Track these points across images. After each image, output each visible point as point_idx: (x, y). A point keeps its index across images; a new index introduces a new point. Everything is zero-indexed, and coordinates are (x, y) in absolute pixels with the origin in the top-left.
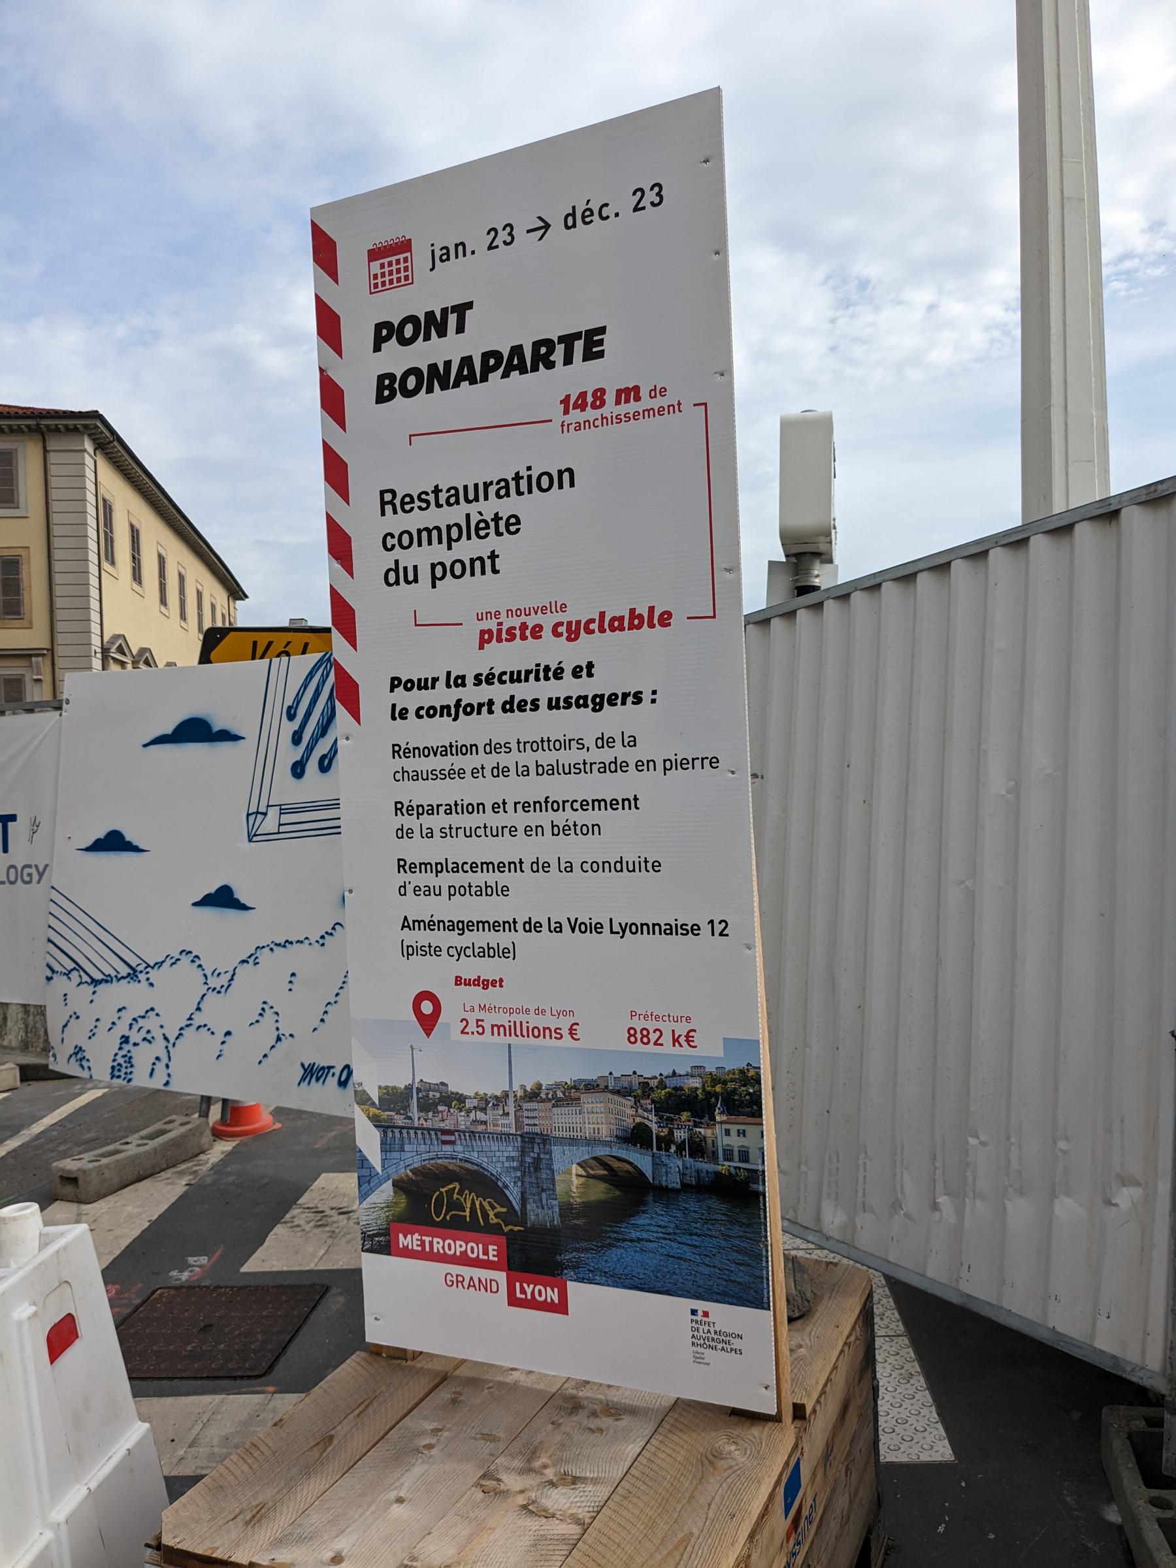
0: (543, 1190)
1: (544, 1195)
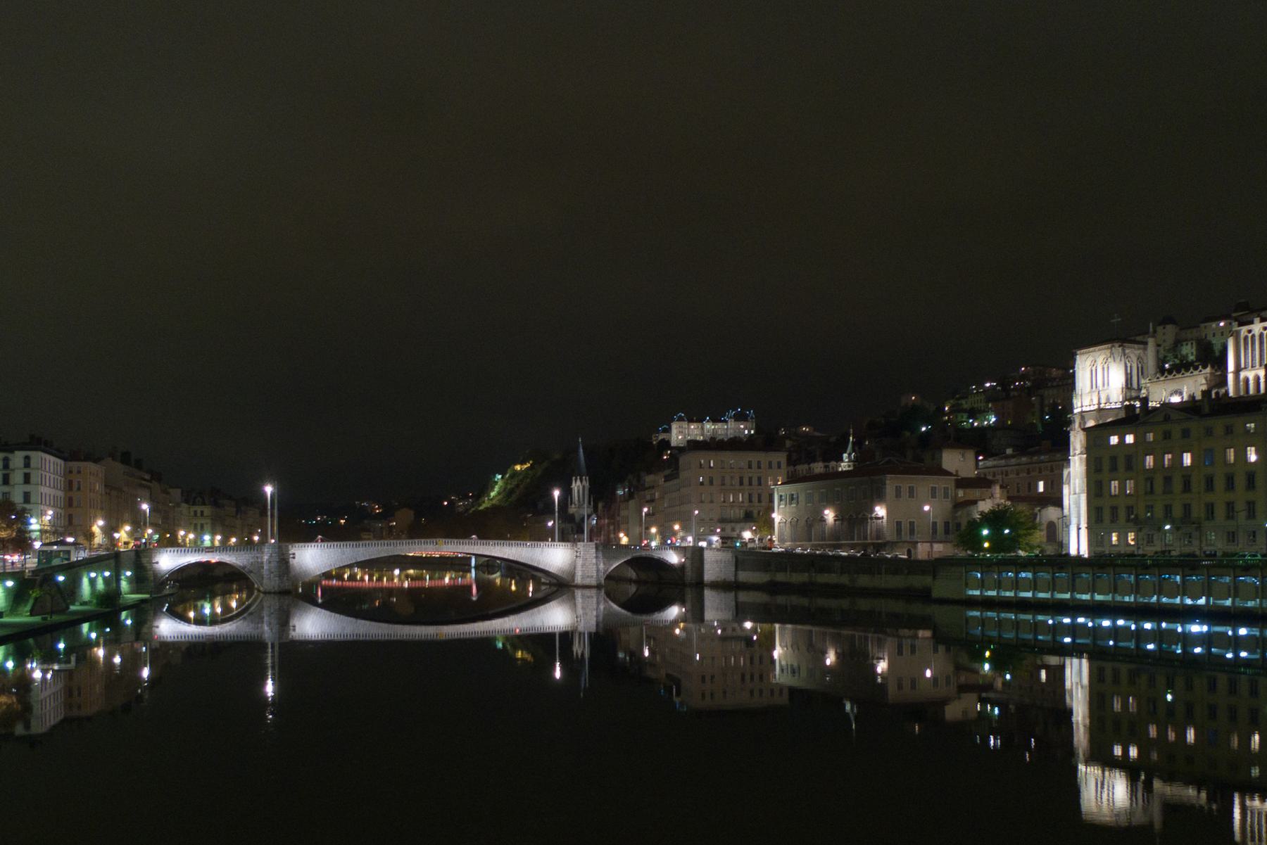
0: (272, 573)
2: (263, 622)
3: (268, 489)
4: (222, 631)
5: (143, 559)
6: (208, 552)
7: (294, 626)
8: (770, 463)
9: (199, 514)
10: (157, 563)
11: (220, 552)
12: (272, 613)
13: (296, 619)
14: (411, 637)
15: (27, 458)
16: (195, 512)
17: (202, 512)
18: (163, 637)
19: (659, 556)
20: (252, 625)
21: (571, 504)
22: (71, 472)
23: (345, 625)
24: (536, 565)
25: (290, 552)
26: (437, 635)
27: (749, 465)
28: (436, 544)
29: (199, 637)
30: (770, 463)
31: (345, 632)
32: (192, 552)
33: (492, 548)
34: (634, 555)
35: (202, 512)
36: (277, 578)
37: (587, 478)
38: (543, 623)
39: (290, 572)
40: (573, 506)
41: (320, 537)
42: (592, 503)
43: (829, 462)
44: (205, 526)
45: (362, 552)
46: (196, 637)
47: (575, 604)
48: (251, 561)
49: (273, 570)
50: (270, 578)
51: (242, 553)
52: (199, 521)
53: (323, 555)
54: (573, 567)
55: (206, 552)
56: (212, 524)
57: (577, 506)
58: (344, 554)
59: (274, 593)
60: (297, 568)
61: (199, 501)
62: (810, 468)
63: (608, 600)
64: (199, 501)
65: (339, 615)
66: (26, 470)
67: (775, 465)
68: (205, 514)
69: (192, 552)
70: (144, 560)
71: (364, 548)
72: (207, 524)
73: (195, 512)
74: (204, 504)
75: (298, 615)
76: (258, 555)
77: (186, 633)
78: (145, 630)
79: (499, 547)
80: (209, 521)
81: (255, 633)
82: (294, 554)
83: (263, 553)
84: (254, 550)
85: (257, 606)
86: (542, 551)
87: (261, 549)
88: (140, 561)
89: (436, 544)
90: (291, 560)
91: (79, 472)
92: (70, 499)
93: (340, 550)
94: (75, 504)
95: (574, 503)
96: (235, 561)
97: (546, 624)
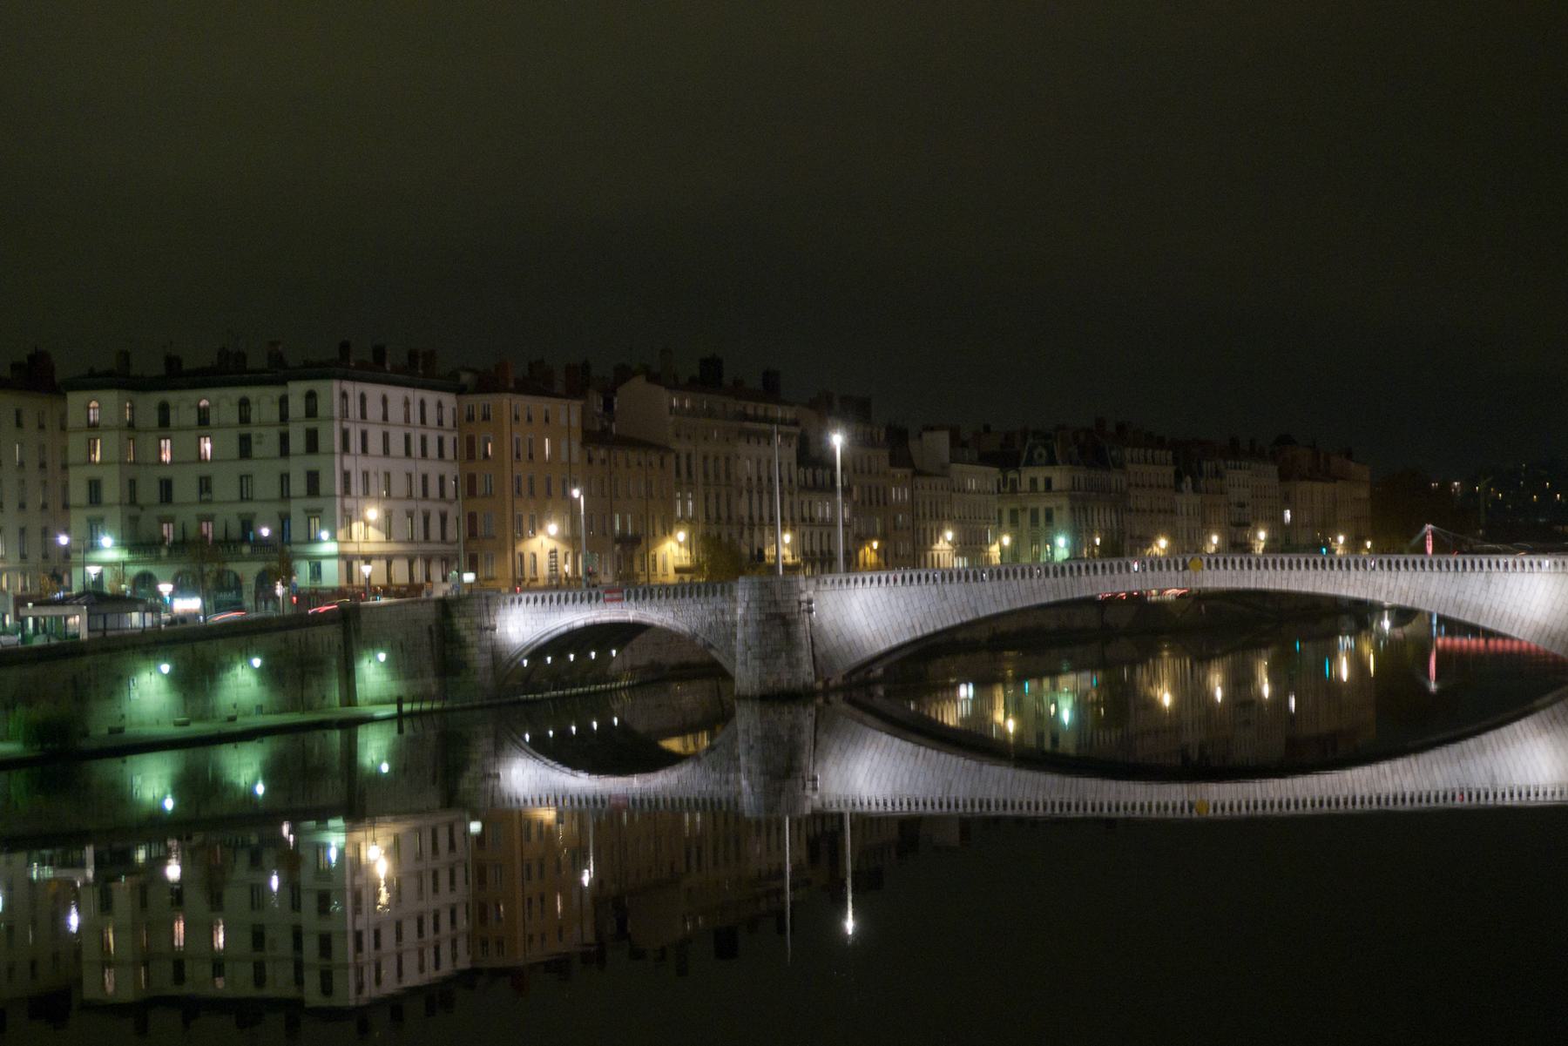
0: (750, 649)
1: (749, 652)
2: (738, 770)
3: (838, 441)
4: (647, 786)
5: (456, 620)
6: (612, 600)
7: (815, 779)
9: (1041, 485)
11: (636, 598)
12: (752, 747)
13: (830, 761)
14: (1549, 797)
15: (244, 403)
16: (1034, 481)
17: (1048, 482)
18: (518, 801)
20: (715, 776)
22: (470, 418)
23: (950, 777)
24: (1468, 619)
26: (1191, 806)
27: (439, 421)
28: (1185, 567)
29: (595, 801)
31: (953, 795)
32: (574, 601)
33: (1340, 574)
35: (1048, 482)
36: (757, 663)
38: (1494, 777)
41: (1429, 527)
44: (1055, 513)
45: (990, 592)
46: (580, 802)
49: (750, 642)
50: (745, 663)
51: (687, 600)
52: (1042, 505)
53: (894, 601)
55: (605, 601)
56: (1072, 509)
58: (946, 597)
59: (753, 698)
60: (832, 637)
61: (1040, 456)
64: (1040, 456)
65: (935, 752)
66: (311, 424)
68: (1055, 486)
69: (574, 601)
70: (460, 623)
72: (1059, 508)
73: (1034, 481)
74: (1052, 462)
75: (835, 750)
76: (726, 606)
77: (567, 791)
78: (465, 784)
79: (1360, 574)
80: (1064, 502)
81: (722, 793)
83: (735, 601)
84: (714, 595)
86: (1489, 583)
87: (731, 591)
88: (452, 625)
89: (1185, 567)
91: (486, 417)
92: (472, 479)
93: (934, 589)
94: (480, 489)
96: (671, 622)
97: (1503, 784)
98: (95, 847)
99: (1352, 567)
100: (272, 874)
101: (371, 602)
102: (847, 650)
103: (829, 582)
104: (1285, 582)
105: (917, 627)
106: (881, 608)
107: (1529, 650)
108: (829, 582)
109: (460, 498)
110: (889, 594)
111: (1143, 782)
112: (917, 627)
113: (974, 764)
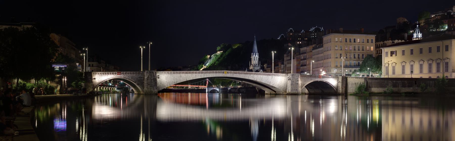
0: (149, 85)
1: (149, 86)
5: (219, 57)
8: (368, 40)
10: (95, 79)
17: (93, 65)
19: (326, 81)
21: (251, 65)
25: (157, 75)
30: (368, 40)
34: (315, 80)
35: (93, 65)
37: (258, 54)
39: (157, 85)
40: (252, 66)
42: (260, 65)
43: (395, 40)
47: (287, 101)
48: (139, 79)
54: (286, 85)
57: (254, 66)
58: (181, 77)
62: (384, 43)
63: (410, 88)
67: (370, 41)
68: (94, 65)
69: (110, 74)
71: (190, 74)
74: (93, 61)
82: (159, 76)
85: (274, 71)
90: (157, 79)
95: (252, 65)
98: (267, 65)
99: (251, 74)
100: (76, 119)
101: (63, 66)
102: (162, 86)
103: (159, 73)
104: (240, 76)
105: (176, 82)
106: (169, 78)
107: (164, 122)
108: (159, 73)
109: (419, 32)
110: (170, 76)
111: (194, 109)
112: (176, 82)
113: (257, 80)
